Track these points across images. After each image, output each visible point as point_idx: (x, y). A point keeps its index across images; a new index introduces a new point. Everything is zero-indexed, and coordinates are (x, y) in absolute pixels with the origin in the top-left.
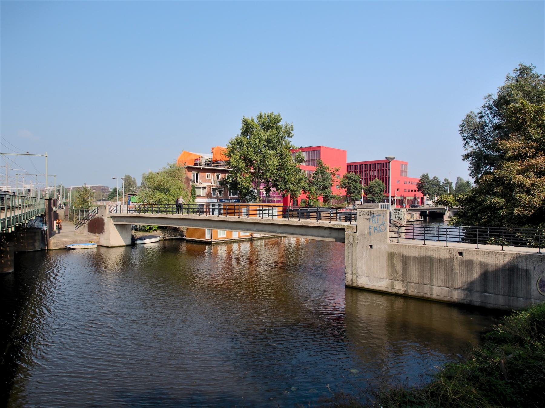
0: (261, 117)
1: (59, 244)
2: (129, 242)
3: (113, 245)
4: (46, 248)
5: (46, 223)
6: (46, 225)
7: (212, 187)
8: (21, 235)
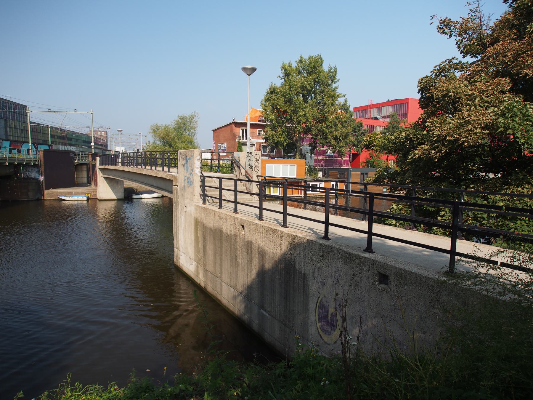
0: (301, 61)
1: (53, 195)
2: (121, 195)
3: (103, 199)
4: (43, 198)
5: (41, 174)
6: (42, 176)
7: (263, 144)
8: (14, 184)
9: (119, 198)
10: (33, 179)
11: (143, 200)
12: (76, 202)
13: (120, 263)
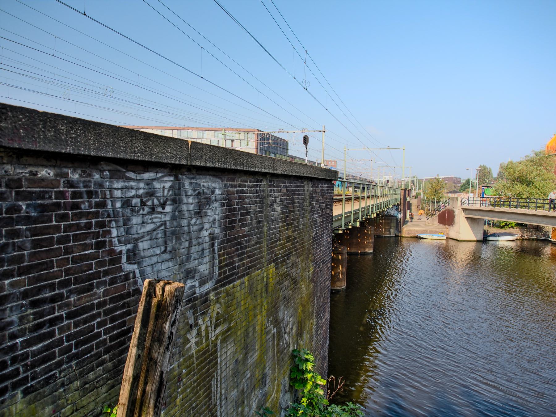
2: (480, 237)
3: (463, 239)
6: (401, 214)
9: (479, 239)
10: (392, 216)
11: (500, 243)
12: (436, 241)
13: (448, 316)
